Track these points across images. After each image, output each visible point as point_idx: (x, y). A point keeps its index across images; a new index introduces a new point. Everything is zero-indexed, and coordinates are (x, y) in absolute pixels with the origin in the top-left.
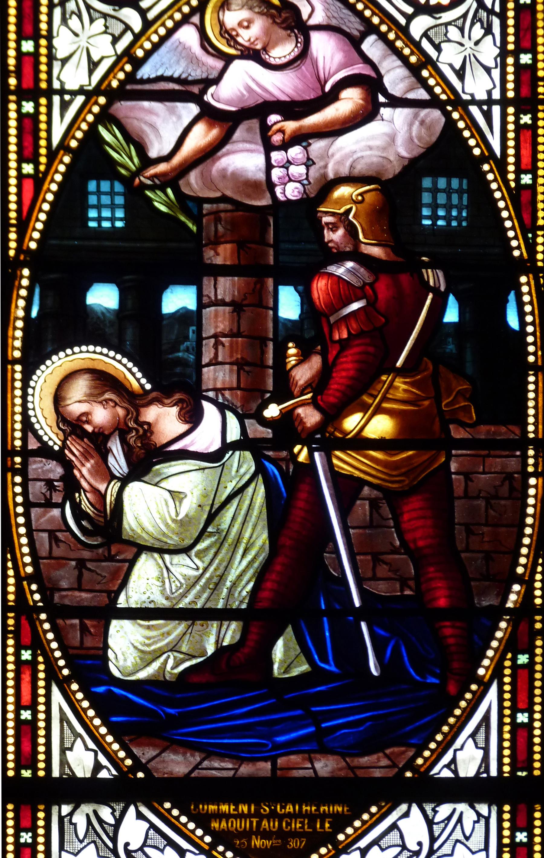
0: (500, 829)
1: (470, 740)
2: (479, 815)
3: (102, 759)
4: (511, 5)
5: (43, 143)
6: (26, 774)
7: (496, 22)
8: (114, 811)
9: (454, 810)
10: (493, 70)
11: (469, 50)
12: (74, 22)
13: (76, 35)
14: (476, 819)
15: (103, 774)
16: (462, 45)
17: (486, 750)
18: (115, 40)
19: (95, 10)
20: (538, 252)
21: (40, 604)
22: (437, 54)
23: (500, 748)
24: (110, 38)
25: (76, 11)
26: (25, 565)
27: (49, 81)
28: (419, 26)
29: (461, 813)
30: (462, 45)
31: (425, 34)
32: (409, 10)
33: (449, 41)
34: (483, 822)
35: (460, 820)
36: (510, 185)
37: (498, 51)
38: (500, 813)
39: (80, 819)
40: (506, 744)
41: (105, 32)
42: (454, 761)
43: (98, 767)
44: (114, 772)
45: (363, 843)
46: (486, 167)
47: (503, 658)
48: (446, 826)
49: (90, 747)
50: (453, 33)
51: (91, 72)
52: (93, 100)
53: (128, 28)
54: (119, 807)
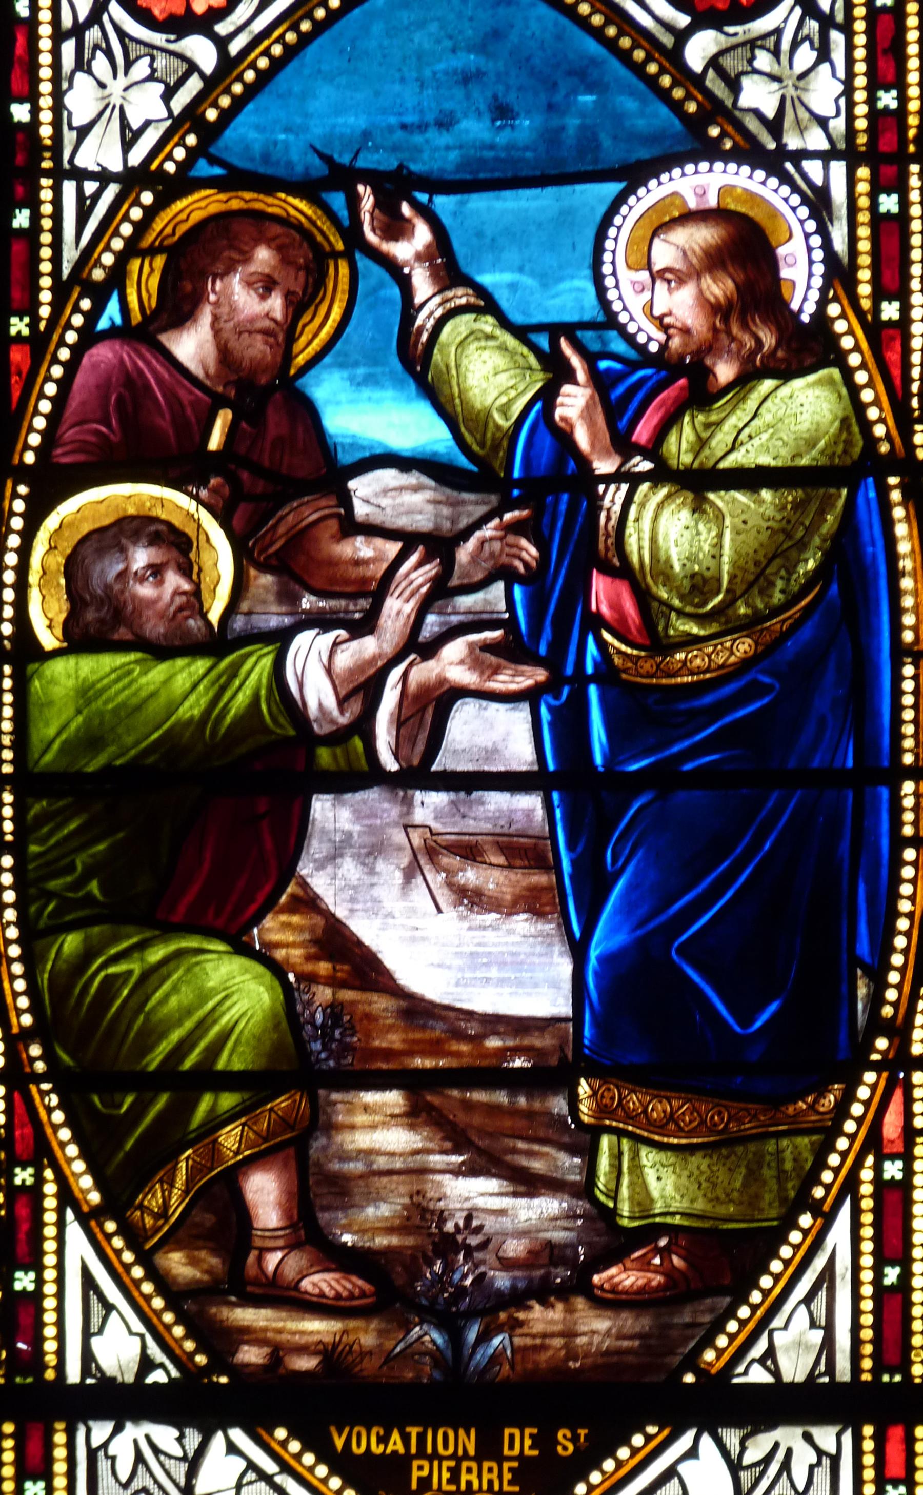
1: (803, 1307)
2: (820, 1453)
3: (155, 1351)
4: (860, 12)
7: (837, 38)
8: (180, 1439)
9: (776, 1445)
12: (100, 64)
13: (102, 86)
14: (814, 1460)
15: (157, 1377)
18: (168, 95)
19: (132, 39)
29: (789, 1452)
31: (714, 62)
32: (683, 20)
33: (756, 71)
34: (826, 1462)
35: (786, 1466)
37: (841, 88)
38: (858, 1440)
43: (146, 1364)
44: (175, 1373)
47: (858, 1164)
48: (763, 1473)
49: (134, 1330)
50: (763, 60)
51: (127, 146)
53: (192, 68)
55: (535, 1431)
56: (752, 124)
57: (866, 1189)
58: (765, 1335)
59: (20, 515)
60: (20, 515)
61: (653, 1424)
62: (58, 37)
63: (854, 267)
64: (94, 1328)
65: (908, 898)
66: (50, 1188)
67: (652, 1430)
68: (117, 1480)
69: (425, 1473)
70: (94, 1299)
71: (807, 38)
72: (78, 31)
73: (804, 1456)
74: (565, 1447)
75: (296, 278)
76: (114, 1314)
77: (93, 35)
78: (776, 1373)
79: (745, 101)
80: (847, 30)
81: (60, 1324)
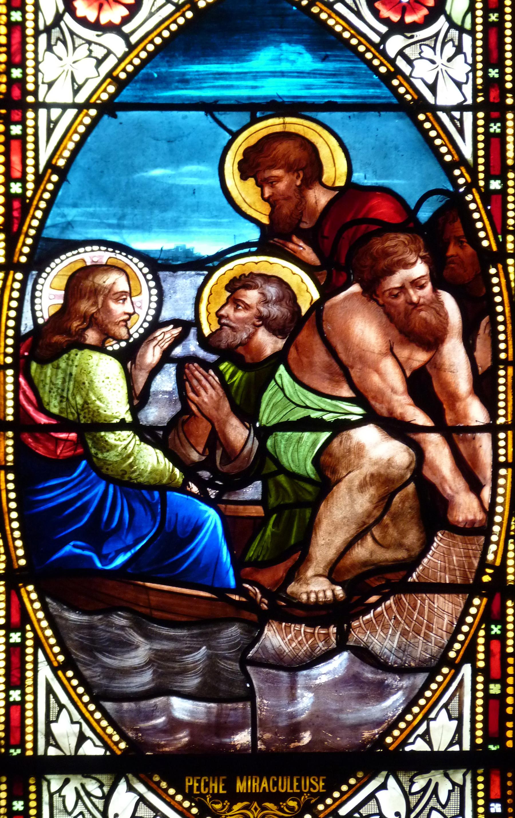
0: (475, 798)
2: (454, 784)
3: (88, 732)
6: (15, 752)
7: (467, 39)
9: (430, 781)
10: (464, 86)
11: (441, 66)
12: (59, 48)
13: (60, 59)
14: (451, 788)
16: (433, 62)
17: (460, 719)
20: (509, 195)
22: (410, 69)
23: (473, 713)
24: (94, 61)
25: (61, 37)
29: (437, 784)
30: (433, 62)
31: (401, 53)
32: (383, 29)
35: (435, 792)
36: (481, 190)
37: (469, 68)
39: (69, 792)
40: (480, 718)
41: (90, 56)
42: (427, 732)
43: (82, 738)
46: (457, 172)
51: (76, 92)
53: (109, 52)
58: (425, 723)
59: (19, 539)
60: (19, 539)
63: (476, 164)
64: (52, 718)
65: (503, 455)
66: (30, 643)
70: (52, 700)
71: (452, 40)
72: (48, 30)
73: (444, 787)
76: (64, 710)
77: (55, 33)
78: (430, 743)
80: (472, 33)
81: (35, 709)
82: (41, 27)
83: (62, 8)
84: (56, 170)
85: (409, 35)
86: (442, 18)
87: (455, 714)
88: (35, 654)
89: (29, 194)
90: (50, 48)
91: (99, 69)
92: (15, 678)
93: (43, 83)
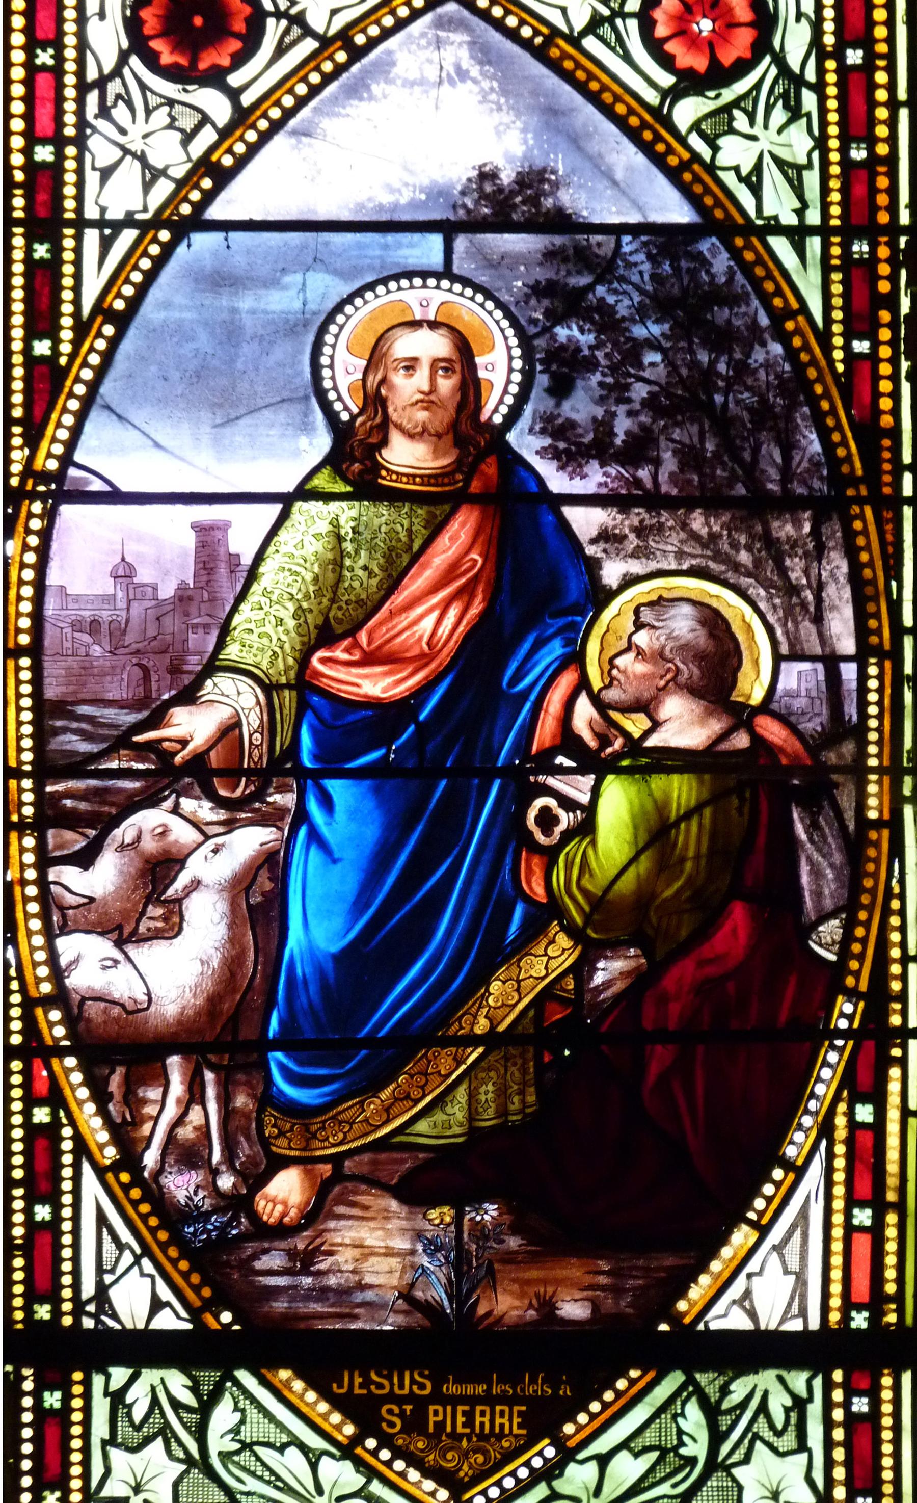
3: (165, 1294)
5: (67, 308)
6: (43, 1312)
7: (809, 100)
12: (120, 113)
21: (67, 1043)
26: (38, 981)
27: (79, 210)
28: (687, 111)
31: (696, 127)
38: (828, 1386)
41: (170, 127)
42: (747, 1294)
43: (157, 1305)
45: (601, 1445)
52: (150, 236)
53: (205, 119)
54: (209, 1377)
55: (524, 1408)
56: (730, 179)
57: (841, 1133)
61: (636, 1367)
62: (83, 88)
67: (634, 1374)
68: (131, 1421)
69: (440, 1418)
72: (102, 83)
73: (778, 1403)
74: (570, 984)
75: (334, 1230)
77: (114, 88)
78: (752, 1315)
79: (722, 159)
80: (819, 88)
81: (76, 1259)
82: (92, 74)
83: (125, 44)
84: (111, 316)
85: (711, 94)
86: (768, 59)
87: (794, 1264)
88: (76, 1166)
89: (842, 1107)
90: (104, 112)
91: (190, 148)
92: (42, 1182)
93: (94, 168)
